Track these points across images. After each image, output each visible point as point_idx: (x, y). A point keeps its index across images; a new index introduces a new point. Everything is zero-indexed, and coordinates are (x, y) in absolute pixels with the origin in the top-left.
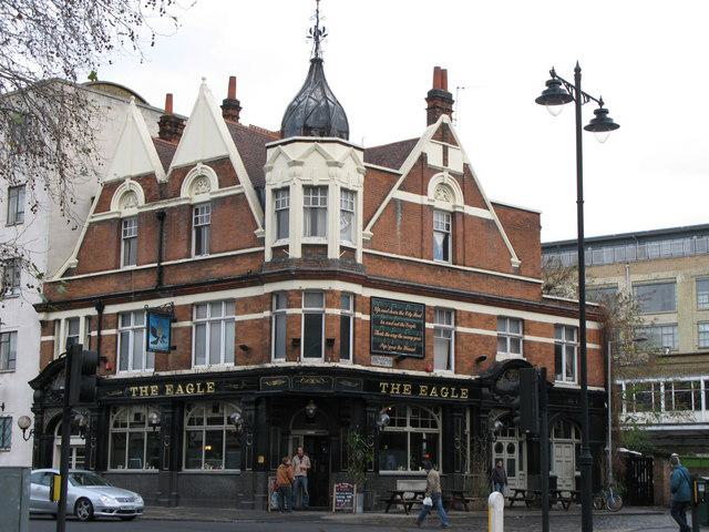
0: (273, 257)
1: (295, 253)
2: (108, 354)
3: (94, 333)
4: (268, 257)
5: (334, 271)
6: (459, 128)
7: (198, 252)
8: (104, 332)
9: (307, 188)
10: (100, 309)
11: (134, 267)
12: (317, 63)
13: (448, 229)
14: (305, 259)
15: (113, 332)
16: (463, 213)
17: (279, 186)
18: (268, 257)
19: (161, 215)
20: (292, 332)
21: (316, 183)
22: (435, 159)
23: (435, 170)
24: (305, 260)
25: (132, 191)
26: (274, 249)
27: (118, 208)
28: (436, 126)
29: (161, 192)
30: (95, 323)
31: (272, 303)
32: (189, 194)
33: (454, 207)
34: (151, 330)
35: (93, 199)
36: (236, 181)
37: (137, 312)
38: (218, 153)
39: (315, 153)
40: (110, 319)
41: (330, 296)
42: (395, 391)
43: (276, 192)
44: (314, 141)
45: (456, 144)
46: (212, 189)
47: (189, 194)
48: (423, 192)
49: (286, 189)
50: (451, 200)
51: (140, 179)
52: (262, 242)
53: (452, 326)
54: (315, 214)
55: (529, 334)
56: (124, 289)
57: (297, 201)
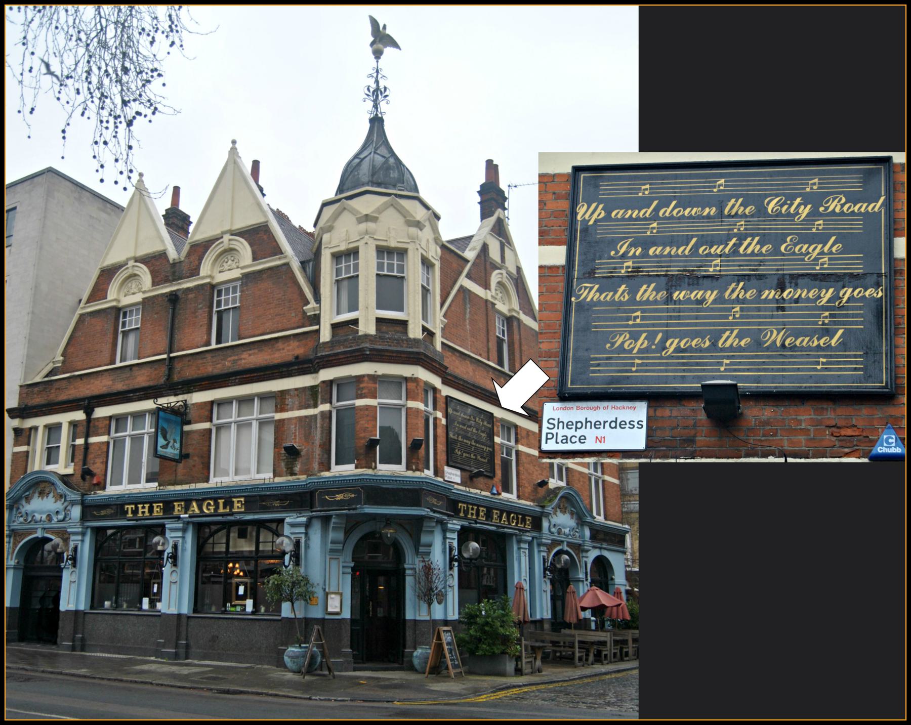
1: (368, 327)
2: (96, 468)
3: (80, 441)
4: (326, 335)
5: (418, 353)
7: (219, 341)
8: (93, 440)
9: (383, 251)
10: (89, 412)
12: (377, 122)
13: (503, 335)
15: (104, 438)
17: (343, 247)
18: (326, 335)
19: (173, 298)
21: (393, 244)
22: (494, 253)
23: (495, 267)
25: (135, 275)
26: (335, 326)
27: (115, 295)
28: (492, 220)
29: (174, 273)
30: (81, 429)
32: (210, 271)
34: (160, 431)
35: (80, 301)
36: (277, 251)
37: (138, 416)
39: (391, 210)
40: (100, 424)
41: (412, 385)
42: (143, 508)
43: (337, 257)
47: (210, 271)
48: (486, 286)
49: (354, 253)
50: (507, 303)
51: (146, 260)
52: (316, 319)
53: (512, 443)
54: (390, 289)
56: (120, 387)
57: (368, 267)
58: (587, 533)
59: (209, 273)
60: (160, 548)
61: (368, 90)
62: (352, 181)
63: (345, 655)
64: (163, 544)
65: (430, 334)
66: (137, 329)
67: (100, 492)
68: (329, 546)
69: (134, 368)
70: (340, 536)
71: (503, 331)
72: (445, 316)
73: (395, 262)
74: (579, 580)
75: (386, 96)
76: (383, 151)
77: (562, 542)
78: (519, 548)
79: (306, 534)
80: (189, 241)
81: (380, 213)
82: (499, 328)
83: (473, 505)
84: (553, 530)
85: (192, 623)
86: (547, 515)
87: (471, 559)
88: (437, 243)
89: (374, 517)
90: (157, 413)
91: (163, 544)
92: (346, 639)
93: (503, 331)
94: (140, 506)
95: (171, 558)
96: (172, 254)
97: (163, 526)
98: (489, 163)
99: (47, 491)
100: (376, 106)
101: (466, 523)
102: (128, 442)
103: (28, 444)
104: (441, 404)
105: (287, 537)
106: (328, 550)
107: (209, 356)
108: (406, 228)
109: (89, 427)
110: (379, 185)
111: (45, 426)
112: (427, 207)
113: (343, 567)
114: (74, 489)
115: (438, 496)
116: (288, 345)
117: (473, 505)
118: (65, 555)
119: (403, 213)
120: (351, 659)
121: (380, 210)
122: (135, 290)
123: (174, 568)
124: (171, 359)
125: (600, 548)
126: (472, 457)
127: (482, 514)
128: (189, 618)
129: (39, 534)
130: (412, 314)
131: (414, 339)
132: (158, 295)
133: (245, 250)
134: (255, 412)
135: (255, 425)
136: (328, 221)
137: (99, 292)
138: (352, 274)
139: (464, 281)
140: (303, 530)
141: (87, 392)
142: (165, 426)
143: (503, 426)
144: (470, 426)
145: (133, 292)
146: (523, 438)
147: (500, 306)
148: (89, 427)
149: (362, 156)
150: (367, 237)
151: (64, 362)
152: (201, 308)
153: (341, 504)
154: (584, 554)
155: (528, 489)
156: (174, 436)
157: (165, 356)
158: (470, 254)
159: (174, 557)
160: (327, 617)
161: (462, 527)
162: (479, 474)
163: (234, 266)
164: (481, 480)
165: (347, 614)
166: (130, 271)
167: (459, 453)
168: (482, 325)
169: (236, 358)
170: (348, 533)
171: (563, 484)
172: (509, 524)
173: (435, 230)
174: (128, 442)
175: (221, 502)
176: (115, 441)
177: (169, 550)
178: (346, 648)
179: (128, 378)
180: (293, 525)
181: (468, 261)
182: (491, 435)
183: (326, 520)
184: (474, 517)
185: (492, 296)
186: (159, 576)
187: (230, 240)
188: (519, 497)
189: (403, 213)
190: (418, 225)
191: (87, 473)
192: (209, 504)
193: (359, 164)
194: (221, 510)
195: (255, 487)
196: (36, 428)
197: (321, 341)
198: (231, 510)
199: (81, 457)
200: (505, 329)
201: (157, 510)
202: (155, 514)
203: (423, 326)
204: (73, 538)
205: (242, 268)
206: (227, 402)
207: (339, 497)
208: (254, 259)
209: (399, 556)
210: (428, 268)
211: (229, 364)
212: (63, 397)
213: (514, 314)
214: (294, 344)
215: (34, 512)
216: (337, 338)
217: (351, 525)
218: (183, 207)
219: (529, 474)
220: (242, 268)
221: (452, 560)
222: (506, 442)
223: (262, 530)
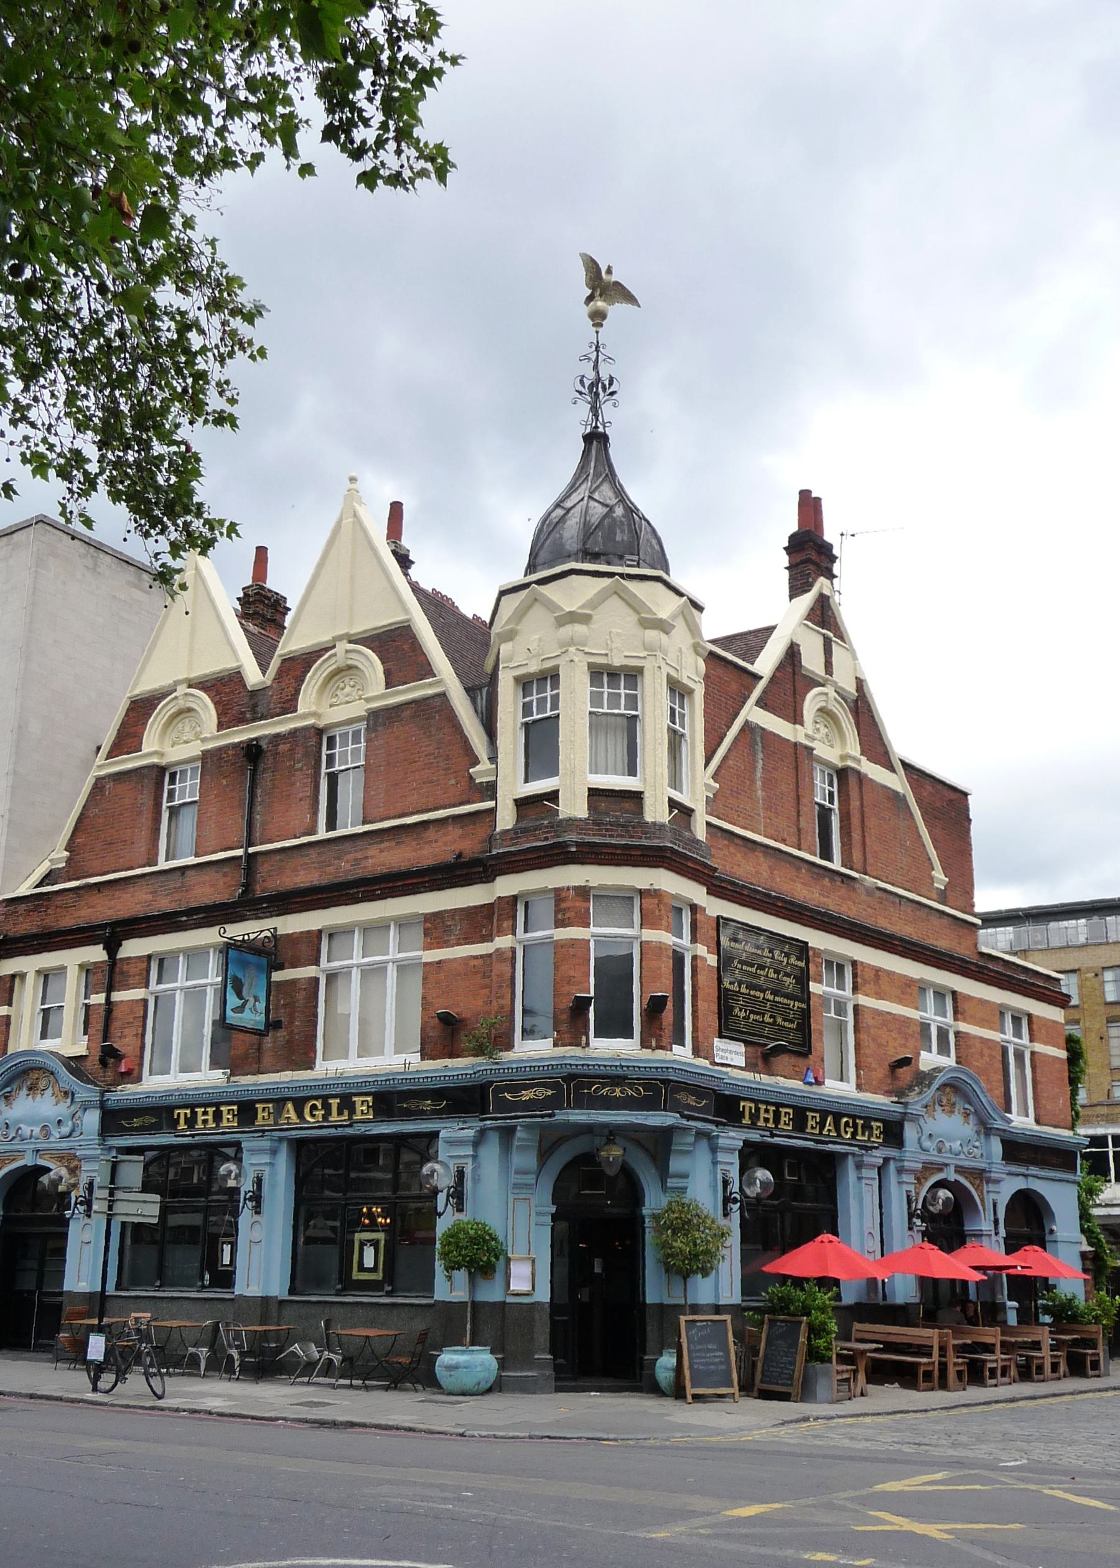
0: (520, 818)
1: (574, 806)
2: (124, 1044)
3: (99, 999)
4: (506, 819)
6: (847, 612)
7: (331, 825)
9: (601, 674)
10: (112, 948)
11: (192, 860)
12: (596, 440)
13: (831, 802)
14: (596, 820)
16: (859, 773)
17: (534, 667)
18: (506, 819)
19: (252, 752)
20: (569, 981)
21: (617, 661)
22: (812, 661)
23: (813, 682)
24: (597, 823)
27: (156, 745)
28: (806, 600)
30: (102, 977)
31: (514, 917)
32: (314, 705)
33: (843, 758)
35: (99, 748)
36: (425, 670)
37: (195, 955)
38: (383, 618)
39: (615, 596)
40: (132, 969)
41: (650, 903)
42: (205, 1113)
43: (525, 684)
44: (611, 575)
45: (842, 638)
46: (373, 686)
47: (314, 705)
48: (796, 718)
49: (551, 677)
52: (490, 790)
53: (848, 992)
55: (964, 1020)
56: (165, 904)
57: (576, 701)
58: (997, 1147)
59: (313, 708)
60: (231, 1183)
61: (582, 382)
62: (549, 553)
63: (541, 1364)
64: (238, 1177)
65: (683, 812)
66: (195, 802)
67: (131, 1088)
68: (514, 1178)
69: (189, 873)
70: (530, 1160)
71: (831, 794)
72: (715, 777)
73: (622, 691)
74: (979, 1235)
75: (612, 393)
76: (606, 493)
77: (947, 1165)
78: (860, 1178)
79: (475, 1157)
80: (278, 652)
81: (594, 608)
82: (821, 789)
83: (767, 1103)
84: (927, 1144)
85: (287, 1312)
86: (915, 1118)
87: (758, 1198)
88: (697, 654)
89: (589, 1129)
90: (229, 948)
91: (238, 1177)
92: (542, 1335)
93: (831, 794)
94: (200, 1110)
95: (250, 1199)
96: (254, 676)
97: (237, 1145)
98: (805, 495)
99: (42, 1084)
100: (595, 410)
101: (754, 1136)
102: (179, 997)
103: (10, 1004)
104: (709, 931)
105: (441, 1163)
106: (511, 1186)
107: (313, 853)
108: (638, 631)
109: (111, 975)
110: (595, 557)
111: (38, 972)
112: (680, 594)
113: (538, 1214)
114: (89, 1081)
115: (697, 1091)
116: (445, 835)
117: (767, 1103)
118: (73, 1195)
119: (634, 605)
120: (550, 1372)
121: (596, 602)
122: (190, 736)
123: (256, 1218)
124: (251, 857)
125: (1026, 1176)
126: (767, 1019)
127: (783, 1119)
128: (282, 1302)
129: (28, 1160)
130: (650, 780)
131: (654, 824)
132: (227, 747)
133: (373, 666)
134: (393, 951)
135: (392, 972)
136: (507, 623)
137: (128, 737)
138: (548, 714)
139: (752, 713)
140: (469, 1151)
141: (110, 912)
142: (240, 975)
143: (829, 964)
144: (761, 967)
145: (184, 740)
146: (865, 982)
147: (822, 750)
148: (111, 975)
149: (568, 504)
150: (572, 649)
151: (69, 861)
152: (301, 769)
153: (531, 1105)
154: (992, 1187)
155: (880, 1072)
156: (255, 988)
157: (239, 852)
158: (765, 664)
159: (257, 1198)
160: (510, 1300)
161: (746, 1143)
162: (778, 1050)
163: (355, 695)
164: (784, 1061)
165: (543, 1295)
166: (182, 703)
167: (742, 1014)
168: (786, 787)
169: (359, 855)
170: (544, 1154)
171: (950, 1061)
172: (839, 1136)
173: (694, 629)
174: (179, 997)
175: (335, 1102)
176: (157, 998)
177: (247, 1186)
178: (543, 1351)
179: (177, 890)
180: (452, 1143)
181: (761, 678)
182: (803, 979)
183: (507, 1133)
184: (771, 1125)
185: (807, 736)
186: (232, 1233)
187: (347, 651)
188: (859, 1087)
189: (634, 605)
190: (663, 626)
191: (109, 1055)
192: (314, 1107)
193: (562, 519)
194: (334, 1117)
195: (391, 1077)
196: (23, 976)
197: (498, 830)
198: (350, 1118)
199: (100, 1026)
200: (835, 790)
201: (229, 1119)
202: (225, 1123)
203: (671, 800)
204: (85, 1166)
205: (368, 700)
206: (346, 931)
207: (527, 1095)
208: (389, 685)
209: (635, 1196)
210: (682, 696)
211: (348, 867)
212: (68, 921)
213: (850, 763)
214: (454, 831)
215: (20, 1121)
216: (524, 824)
217: (548, 1145)
218: (272, 583)
219: (880, 1046)
220: (368, 700)
221: (727, 1200)
222: (835, 991)
223: (403, 1150)
